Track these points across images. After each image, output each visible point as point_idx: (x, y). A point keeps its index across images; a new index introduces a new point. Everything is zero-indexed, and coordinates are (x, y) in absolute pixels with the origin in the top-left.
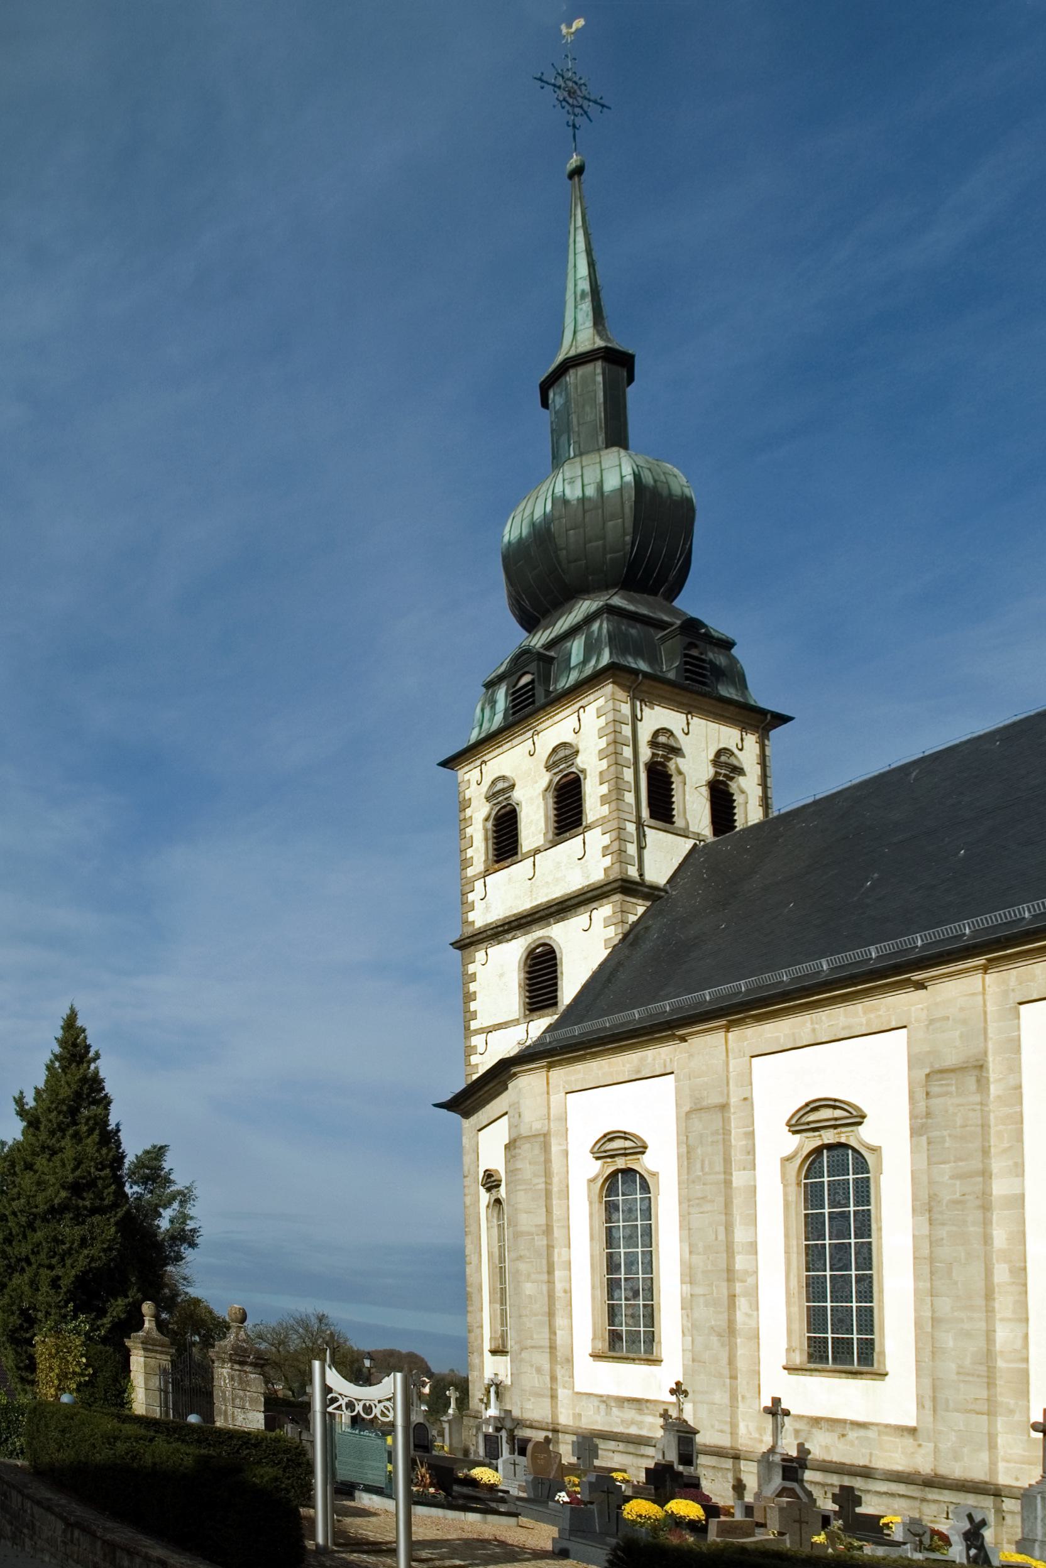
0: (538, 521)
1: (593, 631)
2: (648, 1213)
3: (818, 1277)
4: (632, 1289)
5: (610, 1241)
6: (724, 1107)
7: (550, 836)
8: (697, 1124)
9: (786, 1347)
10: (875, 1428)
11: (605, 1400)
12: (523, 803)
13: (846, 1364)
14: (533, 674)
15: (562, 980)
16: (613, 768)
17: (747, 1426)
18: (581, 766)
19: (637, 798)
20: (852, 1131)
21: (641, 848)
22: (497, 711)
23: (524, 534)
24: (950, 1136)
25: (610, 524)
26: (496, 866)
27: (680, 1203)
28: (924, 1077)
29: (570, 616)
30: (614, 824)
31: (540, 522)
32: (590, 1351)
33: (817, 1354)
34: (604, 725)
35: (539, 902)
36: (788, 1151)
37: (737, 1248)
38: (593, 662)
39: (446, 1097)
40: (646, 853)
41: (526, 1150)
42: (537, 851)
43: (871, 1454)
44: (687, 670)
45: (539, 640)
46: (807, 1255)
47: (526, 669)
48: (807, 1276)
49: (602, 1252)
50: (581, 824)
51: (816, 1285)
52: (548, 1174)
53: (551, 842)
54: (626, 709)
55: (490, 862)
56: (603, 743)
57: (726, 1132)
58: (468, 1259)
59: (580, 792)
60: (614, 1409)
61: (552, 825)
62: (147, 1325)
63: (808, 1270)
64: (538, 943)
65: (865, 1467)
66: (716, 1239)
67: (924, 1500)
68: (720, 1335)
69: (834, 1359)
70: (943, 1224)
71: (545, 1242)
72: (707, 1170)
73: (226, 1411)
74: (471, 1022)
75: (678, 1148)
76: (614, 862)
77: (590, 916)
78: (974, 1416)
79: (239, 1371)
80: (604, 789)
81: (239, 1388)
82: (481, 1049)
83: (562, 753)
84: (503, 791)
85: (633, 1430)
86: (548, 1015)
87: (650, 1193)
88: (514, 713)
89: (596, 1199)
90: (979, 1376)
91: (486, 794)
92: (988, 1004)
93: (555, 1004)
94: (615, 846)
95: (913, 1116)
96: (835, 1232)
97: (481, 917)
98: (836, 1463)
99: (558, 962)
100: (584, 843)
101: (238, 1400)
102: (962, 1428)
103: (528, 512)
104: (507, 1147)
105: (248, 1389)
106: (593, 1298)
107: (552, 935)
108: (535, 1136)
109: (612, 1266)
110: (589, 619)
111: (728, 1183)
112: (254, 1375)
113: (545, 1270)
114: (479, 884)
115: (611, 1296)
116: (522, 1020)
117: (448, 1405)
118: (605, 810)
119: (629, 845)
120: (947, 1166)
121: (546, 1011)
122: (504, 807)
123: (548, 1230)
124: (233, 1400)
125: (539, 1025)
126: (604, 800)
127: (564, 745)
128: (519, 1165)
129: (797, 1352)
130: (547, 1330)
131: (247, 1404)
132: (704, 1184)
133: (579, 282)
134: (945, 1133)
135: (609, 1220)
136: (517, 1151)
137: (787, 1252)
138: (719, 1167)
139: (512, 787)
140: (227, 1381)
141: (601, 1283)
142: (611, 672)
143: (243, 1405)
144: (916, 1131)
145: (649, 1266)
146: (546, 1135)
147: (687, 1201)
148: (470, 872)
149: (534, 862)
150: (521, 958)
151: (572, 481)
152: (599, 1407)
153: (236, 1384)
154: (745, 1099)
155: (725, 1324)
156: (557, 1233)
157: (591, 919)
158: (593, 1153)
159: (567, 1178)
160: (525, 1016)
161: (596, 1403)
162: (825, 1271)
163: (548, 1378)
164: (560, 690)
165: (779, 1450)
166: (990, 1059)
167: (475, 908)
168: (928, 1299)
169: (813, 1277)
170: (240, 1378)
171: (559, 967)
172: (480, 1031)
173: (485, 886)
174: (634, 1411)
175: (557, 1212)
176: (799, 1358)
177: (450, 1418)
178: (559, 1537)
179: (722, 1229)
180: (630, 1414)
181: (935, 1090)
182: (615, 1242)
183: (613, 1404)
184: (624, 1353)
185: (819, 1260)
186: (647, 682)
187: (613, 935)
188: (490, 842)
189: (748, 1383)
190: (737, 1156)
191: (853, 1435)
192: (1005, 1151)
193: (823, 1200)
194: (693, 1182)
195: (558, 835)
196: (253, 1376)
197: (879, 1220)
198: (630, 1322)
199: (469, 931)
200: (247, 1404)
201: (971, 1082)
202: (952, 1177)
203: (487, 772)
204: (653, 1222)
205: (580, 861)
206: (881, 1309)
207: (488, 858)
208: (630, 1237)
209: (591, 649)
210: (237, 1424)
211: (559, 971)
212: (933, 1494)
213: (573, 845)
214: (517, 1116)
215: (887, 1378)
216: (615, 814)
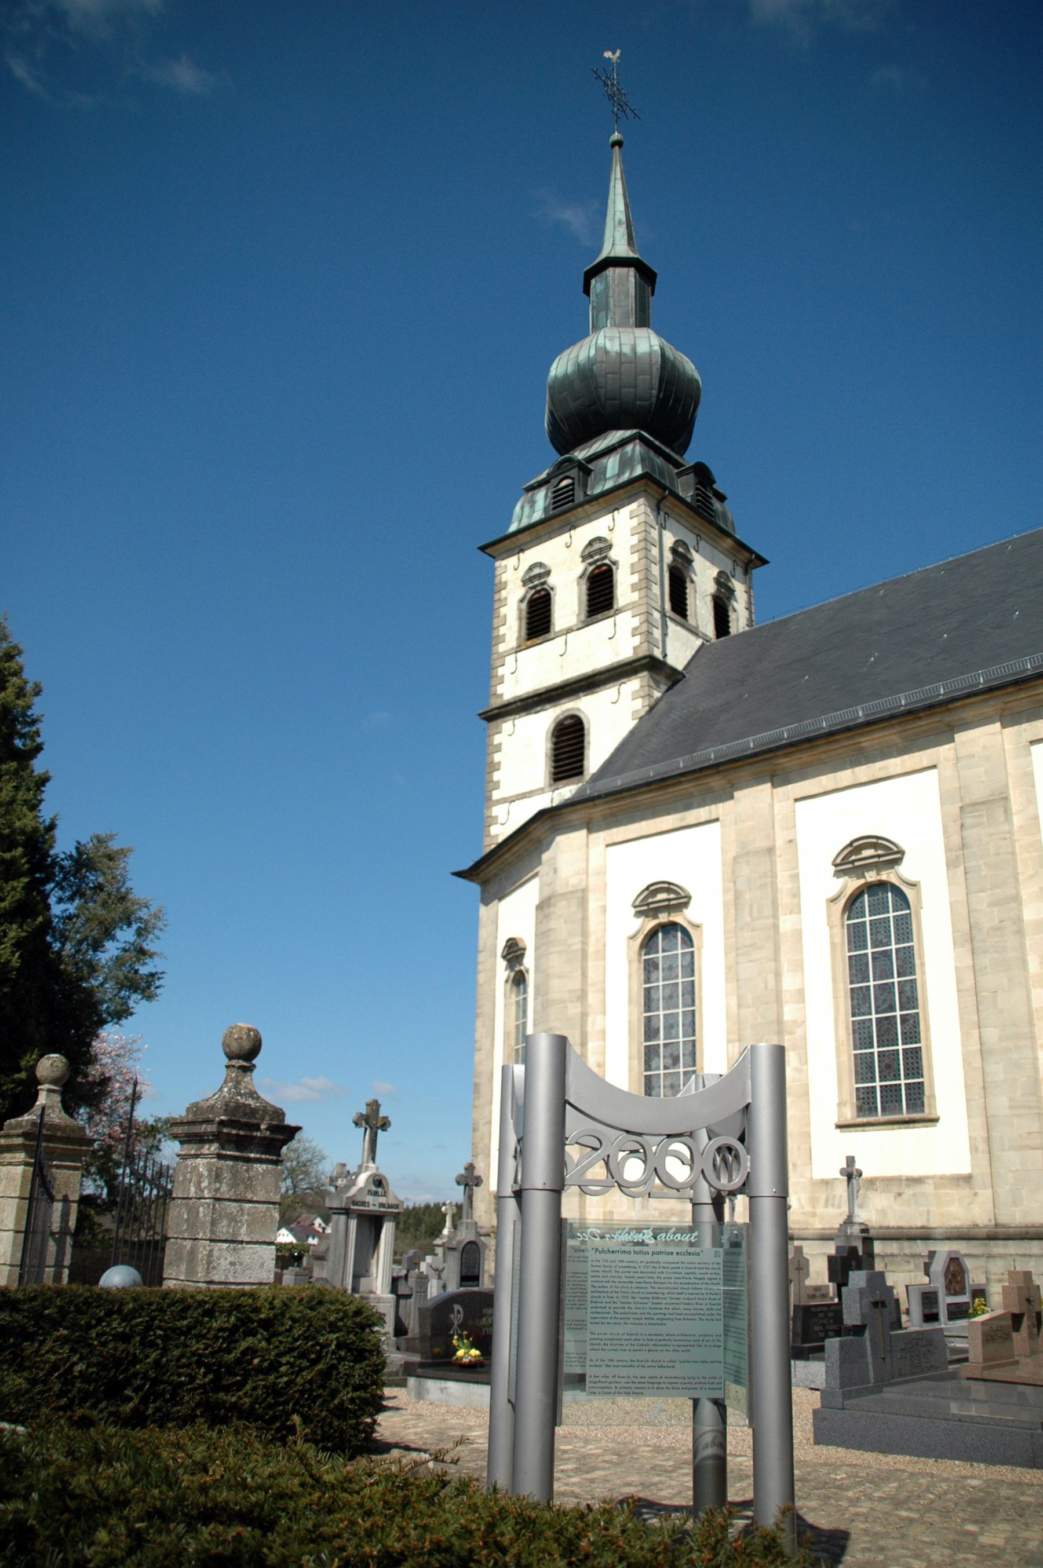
2: (690, 969)
3: (864, 1021)
4: (671, 1055)
5: (649, 1002)
6: (771, 850)
7: (583, 617)
8: (745, 870)
9: (837, 1101)
10: (931, 1181)
13: (894, 1114)
14: (573, 479)
16: (643, 561)
17: (799, 1199)
19: (661, 591)
21: (665, 635)
23: (570, 371)
24: (985, 864)
25: (641, 377)
26: (529, 643)
27: (726, 954)
28: (958, 810)
30: (644, 609)
33: (866, 1106)
36: (833, 892)
37: (785, 997)
39: (466, 865)
40: (668, 640)
41: (561, 909)
42: (569, 630)
43: (928, 1212)
44: (698, 501)
46: (852, 999)
47: (567, 474)
48: (853, 1022)
49: (639, 1014)
51: (862, 1031)
52: (584, 933)
53: (583, 622)
56: (635, 540)
57: (774, 875)
58: (478, 1045)
59: (612, 581)
61: (585, 608)
62: (42, 1099)
63: (853, 1015)
65: (923, 1227)
67: (990, 1256)
69: (883, 1109)
70: (985, 952)
71: (579, 1010)
72: (755, 915)
73: (193, 1252)
78: (1030, 1152)
80: (635, 578)
81: (231, 1195)
82: (501, 820)
84: (539, 576)
86: (573, 783)
87: (692, 946)
88: (554, 509)
89: (635, 956)
90: (1030, 1108)
92: (1005, 743)
93: (581, 773)
94: (644, 628)
95: (948, 849)
96: (878, 973)
97: (509, 690)
98: (893, 1228)
99: (586, 732)
101: (225, 1222)
102: (1019, 1168)
103: (573, 355)
104: (539, 907)
105: (249, 1196)
106: (630, 1069)
108: (572, 892)
109: (650, 1031)
110: (623, 443)
111: (776, 927)
112: (264, 1166)
114: (510, 660)
115: (648, 1066)
116: (547, 789)
117: (443, 1225)
118: (635, 596)
119: (655, 630)
121: (572, 779)
122: (538, 592)
123: (582, 996)
124: (214, 1223)
125: (567, 791)
126: (634, 588)
127: (599, 539)
128: (553, 924)
129: (848, 1106)
131: (243, 1230)
132: (753, 931)
133: (618, 213)
134: (981, 862)
135: (648, 980)
136: (552, 909)
137: (835, 997)
138: (768, 911)
139: (548, 573)
140: (205, 1184)
141: (639, 1051)
142: (644, 481)
143: (234, 1234)
145: (691, 1026)
146: (584, 891)
148: (502, 648)
151: (612, 339)
153: (224, 1188)
154: (790, 841)
156: (592, 998)
158: (635, 907)
159: (604, 936)
160: (550, 785)
162: (870, 1014)
165: (856, 1220)
166: (1011, 792)
168: (976, 1032)
169: (859, 1022)
170: (235, 1174)
175: (592, 974)
176: (849, 1114)
177: (445, 1240)
178: (822, 1407)
179: (771, 977)
181: (968, 821)
182: (653, 1005)
184: (905, 1115)
185: (864, 1003)
186: (670, 498)
188: (524, 621)
189: (799, 1148)
190: (784, 899)
191: (908, 1192)
192: (1031, 877)
193: (865, 941)
194: (741, 929)
195: (589, 616)
196: (261, 1168)
197: (921, 957)
199: (495, 703)
200: (243, 1230)
201: (1000, 813)
202: (989, 905)
204: (696, 978)
206: (929, 1047)
208: (671, 997)
209: (625, 464)
210: (216, 1278)
212: (998, 1248)
213: (603, 627)
214: (551, 872)
215: (939, 1124)
216: (644, 600)
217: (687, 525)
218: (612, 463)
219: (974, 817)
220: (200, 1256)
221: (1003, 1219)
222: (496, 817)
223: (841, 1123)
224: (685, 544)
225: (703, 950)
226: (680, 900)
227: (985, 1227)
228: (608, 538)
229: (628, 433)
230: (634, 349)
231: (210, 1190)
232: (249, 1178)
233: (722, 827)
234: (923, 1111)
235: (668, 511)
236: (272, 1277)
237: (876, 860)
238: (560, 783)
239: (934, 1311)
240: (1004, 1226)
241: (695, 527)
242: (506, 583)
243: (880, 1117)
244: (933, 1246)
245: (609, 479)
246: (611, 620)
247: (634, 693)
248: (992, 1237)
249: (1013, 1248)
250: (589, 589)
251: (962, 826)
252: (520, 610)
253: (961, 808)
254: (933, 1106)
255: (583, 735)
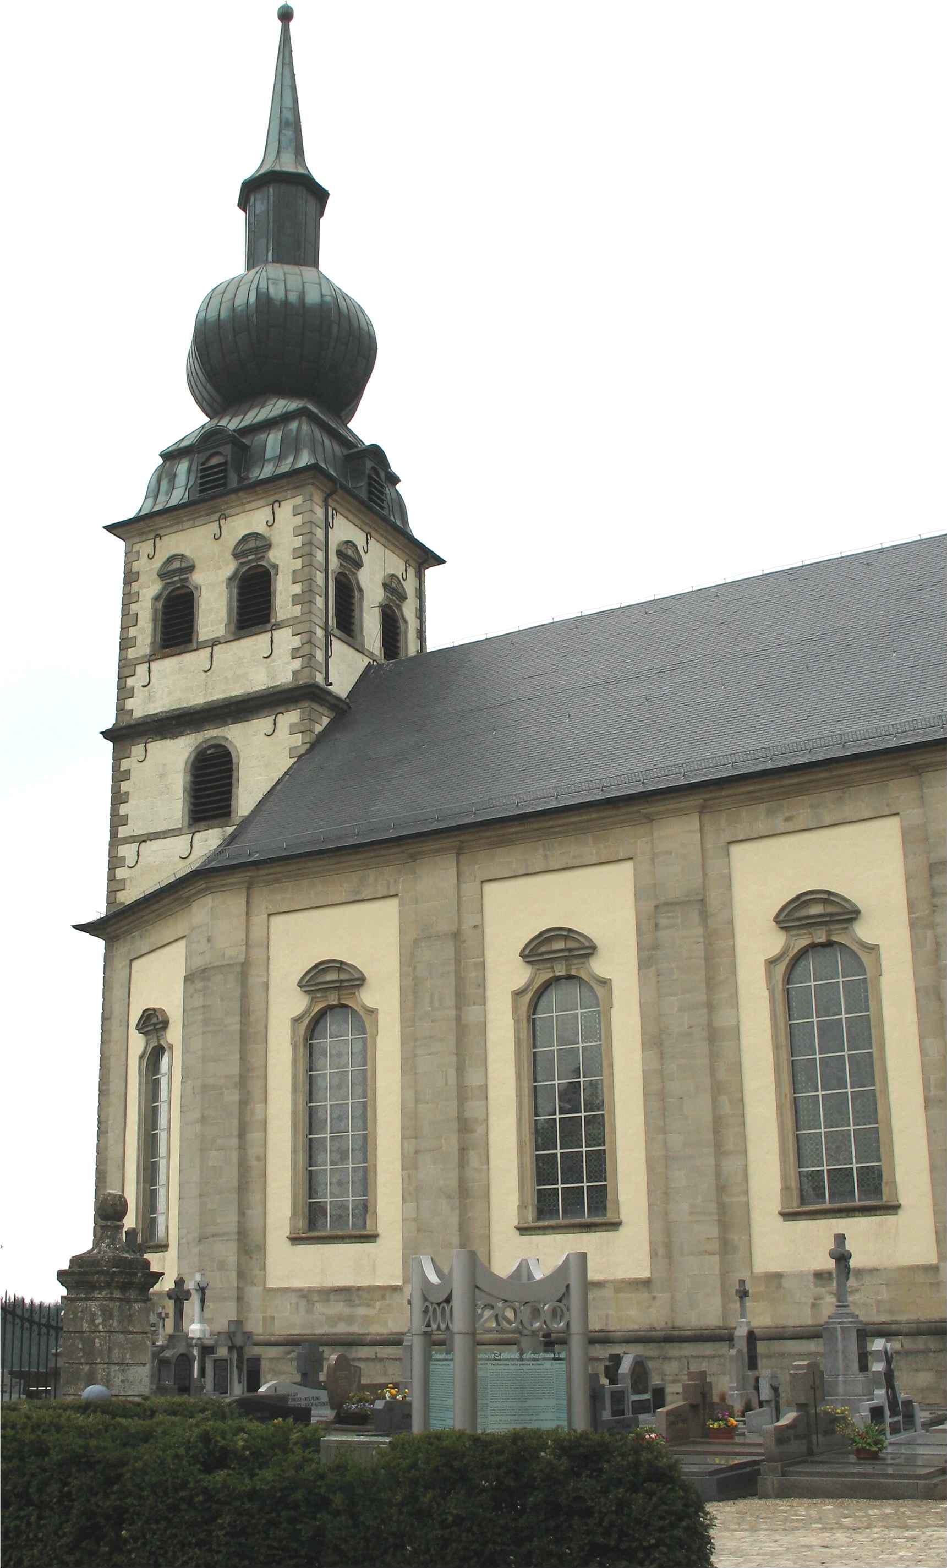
0: (240, 308)
1: (291, 430)
11: (306, 1295)
12: (203, 588)
15: (238, 788)
18: (273, 560)
19: (325, 604)
20: (583, 963)
21: (327, 657)
22: (176, 485)
23: (223, 315)
29: (262, 410)
31: (242, 311)
32: (515, 1222)
34: (301, 524)
35: (215, 698)
38: (290, 460)
42: (215, 642)
43: (607, 1316)
45: (232, 424)
50: (268, 621)
54: (319, 512)
55: (157, 646)
60: (317, 1305)
64: (210, 743)
66: (446, 1084)
68: (449, 1197)
72: (436, 1004)
74: (120, 828)
75: (401, 981)
76: (304, 666)
77: (275, 720)
78: (707, 1257)
79: (120, 1300)
82: (130, 861)
83: (252, 544)
85: (342, 1328)
88: (201, 491)
91: (159, 572)
95: (640, 948)
100: (272, 641)
107: (229, 737)
110: (286, 418)
113: (236, 1133)
120: (676, 998)
126: (296, 600)
127: (255, 535)
129: (530, 1208)
130: (234, 1208)
132: (433, 1021)
138: (450, 1001)
139: (191, 568)
140: (99, 1320)
144: (644, 964)
147: (410, 1040)
149: (212, 653)
150: (189, 758)
152: (297, 1304)
154: (475, 927)
155: (454, 1183)
157: (275, 724)
160: (190, 825)
161: (294, 1300)
163: (234, 1275)
164: (254, 480)
167: (135, 695)
171: (234, 774)
172: (131, 840)
173: (149, 672)
174: (342, 1303)
176: (530, 1215)
179: (452, 1073)
180: (337, 1308)
181: (663, 922)
183: (316, 1298)
184: (587, 1219)
186: (340, 492)
187: (300, 744)
198: (336, 1190)
201: (695, 916)
203: (161, 547)
205: (265, 660)
207: (155, 640)
211: (234, 777)
212: (674, 1350)
213: (258, 643)
215: (900, 1212)
217: (358, 522)
218: (273, 440)
219: (669, 917)
220: (99, 1376)
221: (679, 1322)
222: (124, 858)
223: (522, 1225)
224: (354, 545)
225: (379, 1039)
226: (357, 981)
227: (662, 1330)
228: (266, 535)
229: (293, 405)
230: (302, 295)
231: (104, 1326)
232: (131, 1315)
233: (401, 904)
234: (605, 1215)
235: (337, 507)
236: (147, 1390)
237: (566, 954)
238: (202, 825)
239: (621, 1407)
240: (680, 1329)
241: (366, 524)
242: (138, 573)
243: (561, 1221)
244: (617, 1350)
245: (269, 460)
246: (266, 637)
247: (292, 726)
248: (668, 1340)
249: (689, 1350)
250: (239, 594)
251: (657, 925)
252: (155, 610)
253: (656, 907)
254: (617, 1211)
255: (231, 770)
